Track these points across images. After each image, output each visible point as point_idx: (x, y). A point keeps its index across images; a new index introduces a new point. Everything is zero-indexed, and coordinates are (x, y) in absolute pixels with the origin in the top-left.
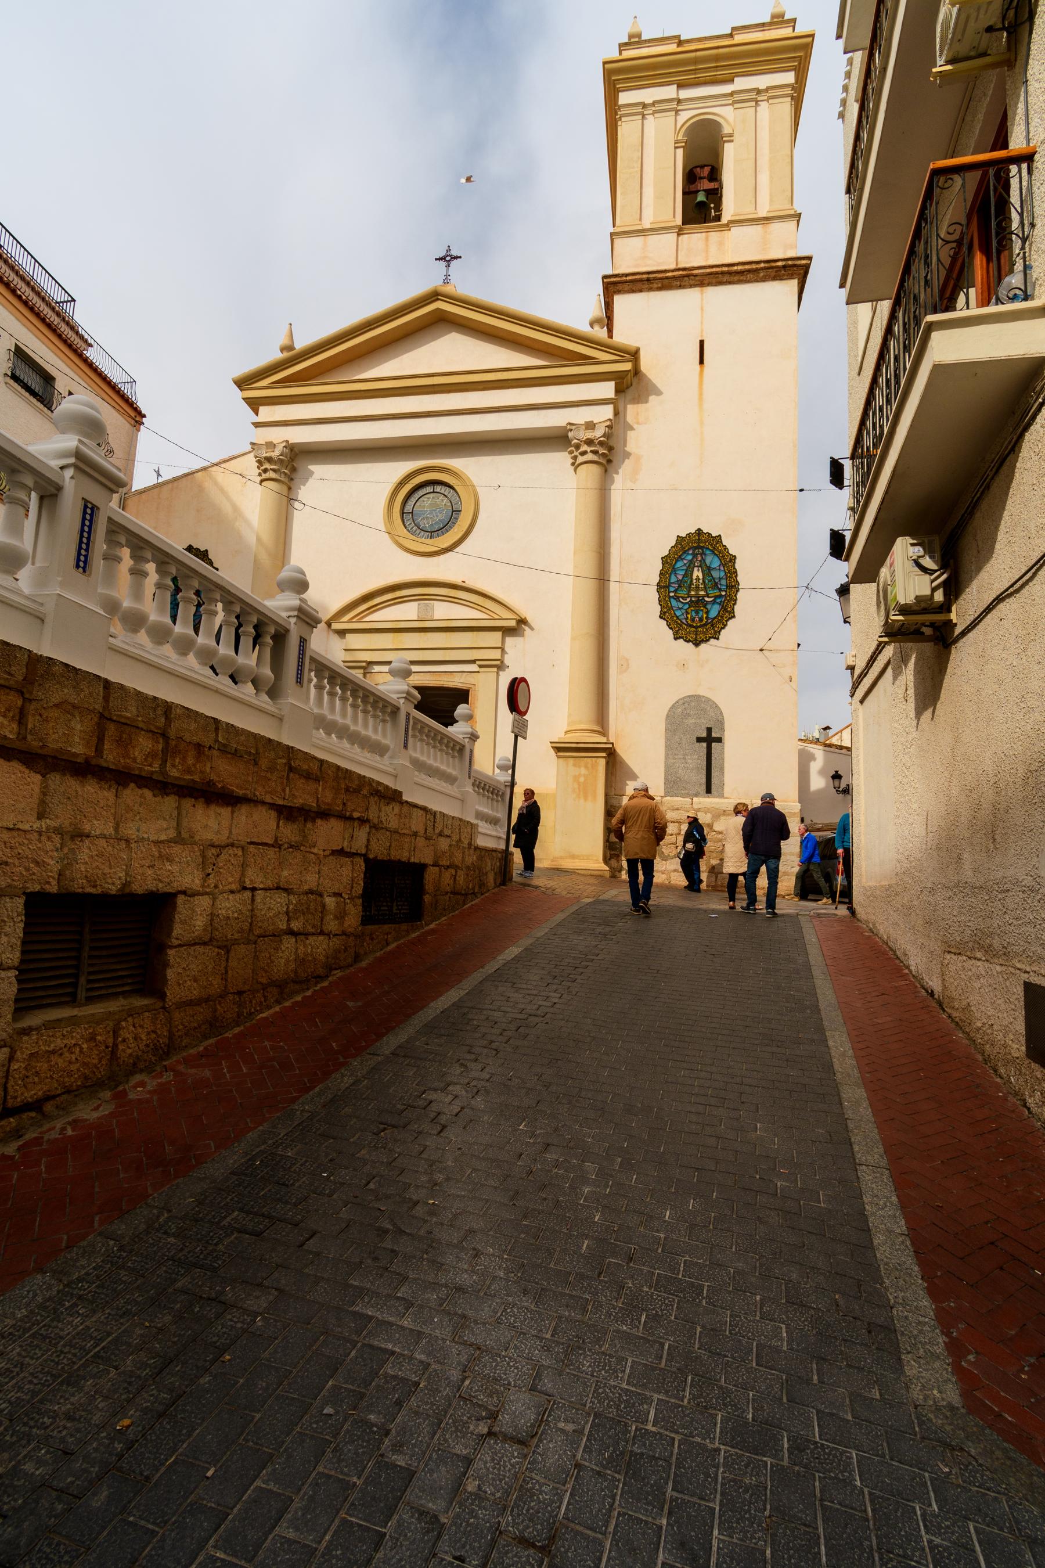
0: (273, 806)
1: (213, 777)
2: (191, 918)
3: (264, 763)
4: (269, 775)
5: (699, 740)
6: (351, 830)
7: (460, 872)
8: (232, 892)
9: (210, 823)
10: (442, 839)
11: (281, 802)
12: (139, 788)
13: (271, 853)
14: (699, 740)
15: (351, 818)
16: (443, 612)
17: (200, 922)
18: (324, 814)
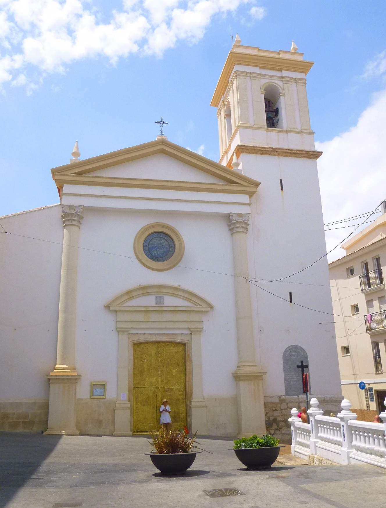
5: (298, 367)
16: (170, 301)
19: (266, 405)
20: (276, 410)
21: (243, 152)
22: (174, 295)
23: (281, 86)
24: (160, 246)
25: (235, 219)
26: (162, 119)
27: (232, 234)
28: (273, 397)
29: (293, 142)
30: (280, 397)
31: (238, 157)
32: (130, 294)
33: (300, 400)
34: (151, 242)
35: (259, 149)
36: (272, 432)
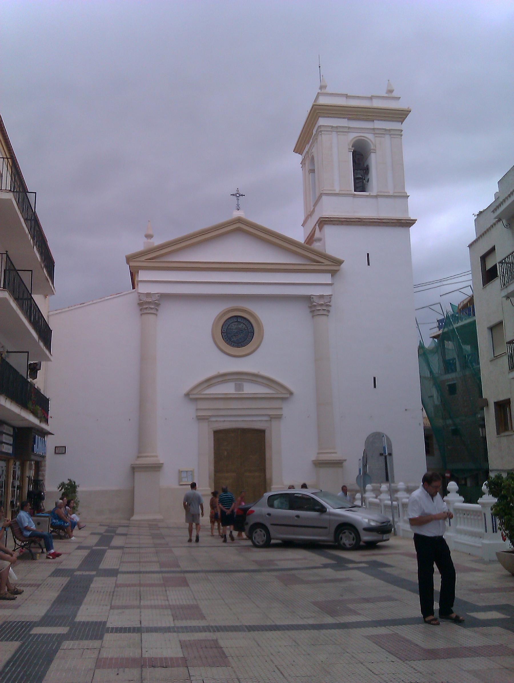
16: (249, 389)
22: (252, 381)
23: (373, 141)
24: (238, 332)
25: (316, 301)
26: (238, 191)
27: (313, 316)
31: (321, 229)
32: (209, 382)
34: (229, 327)
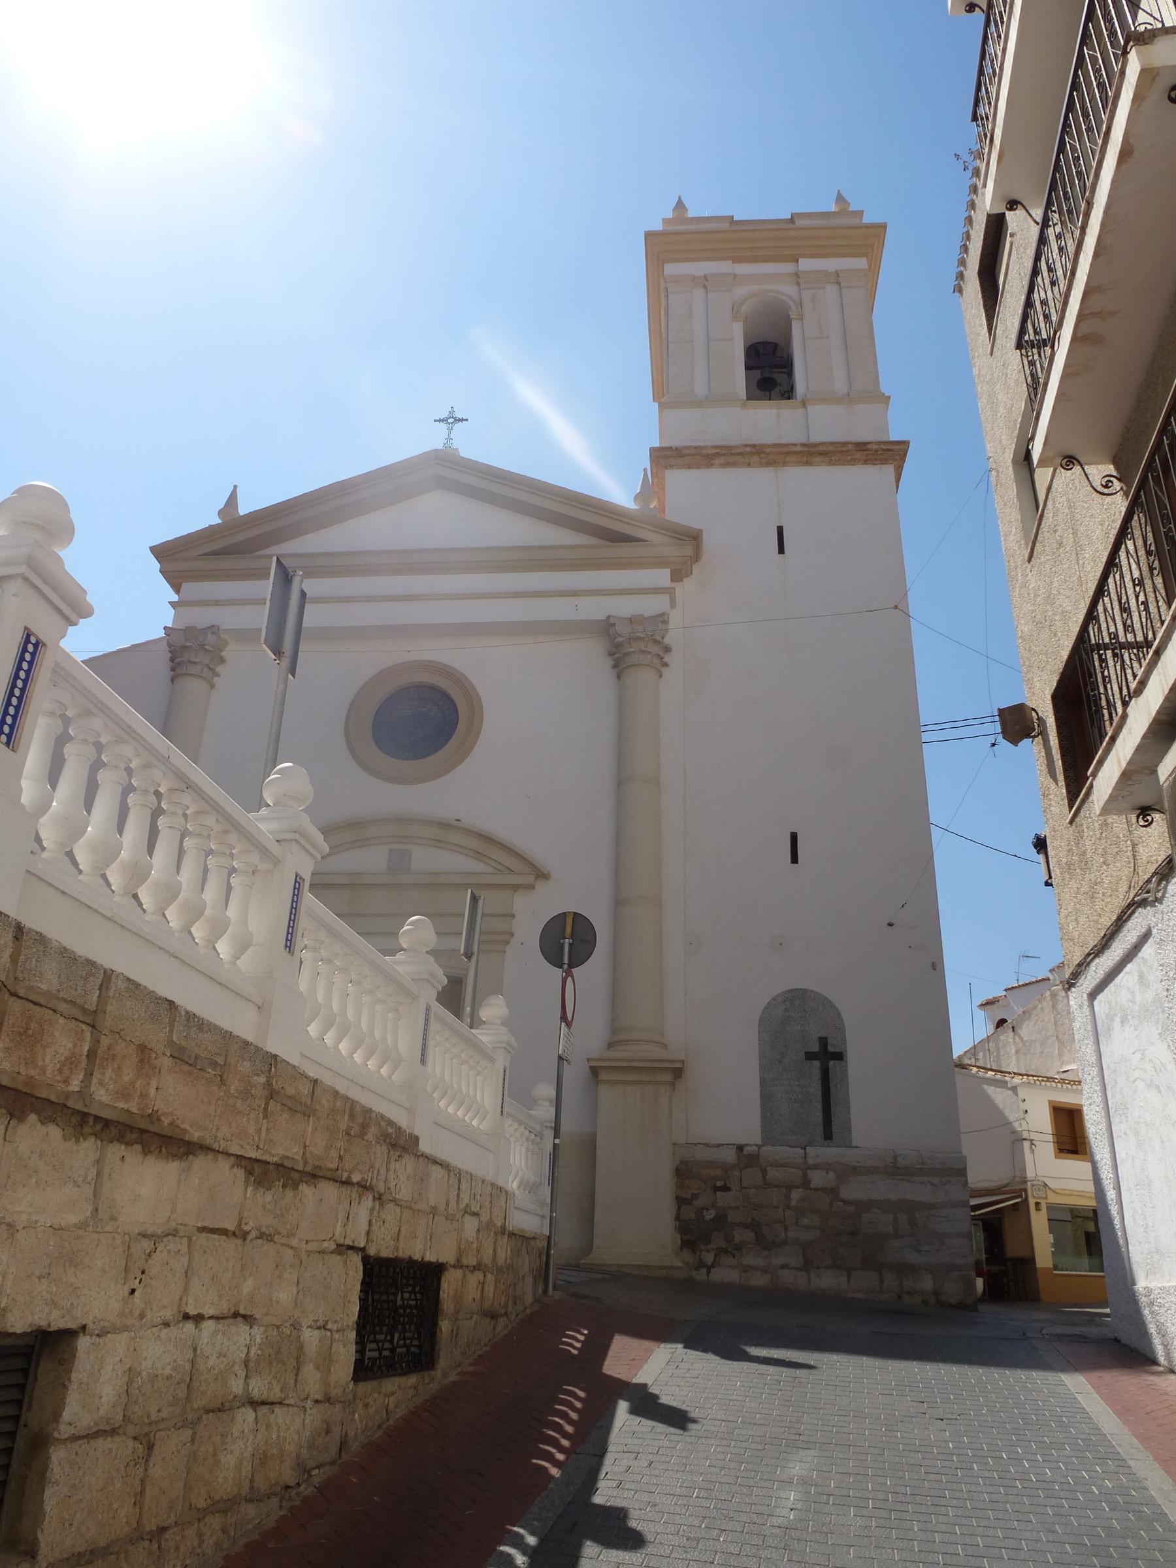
0: (240, 1160)
1: (159, 1105)
2: (94, 1386)
3: (234, 1085)
4: (239, 1104)
5: (810, 1056)
6: (346, 1204)
7: (490, 1277)
8: (166, 1324)
9: (146, 1188)
10: (467, 1218)
11: (253, 1154)
12: (43, 1123)
13: (230, 1246)
14: (810, 1056)
15: (348, 1183)
17: (108, 1393)
18: (313, 1176)
19: (683, 1172)
20: (726, 1189)
21: (671, 467)
22: (440, 844)
25: (623, 629)
28: (719, 1146)
29: (825, 423)
30: (740, 1148)
33: (811, 1161)
35: (714, 451)
36: (709, 1258)
